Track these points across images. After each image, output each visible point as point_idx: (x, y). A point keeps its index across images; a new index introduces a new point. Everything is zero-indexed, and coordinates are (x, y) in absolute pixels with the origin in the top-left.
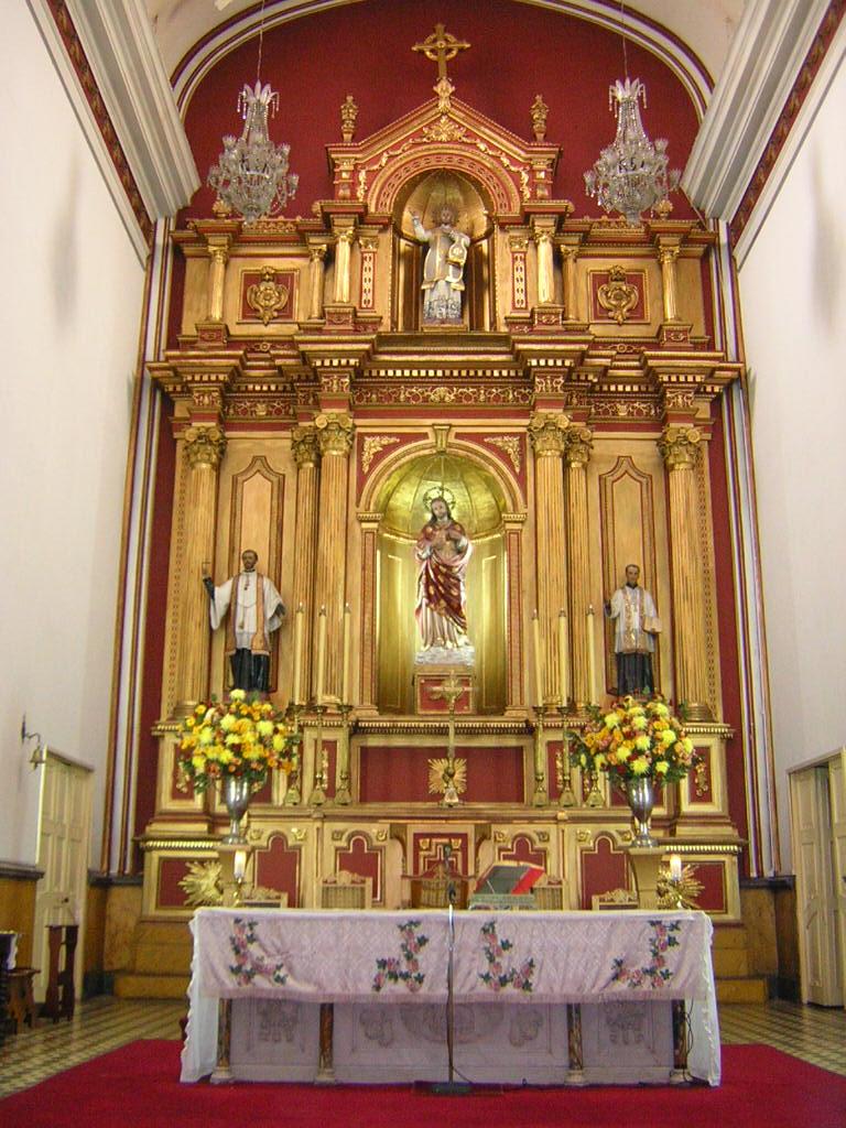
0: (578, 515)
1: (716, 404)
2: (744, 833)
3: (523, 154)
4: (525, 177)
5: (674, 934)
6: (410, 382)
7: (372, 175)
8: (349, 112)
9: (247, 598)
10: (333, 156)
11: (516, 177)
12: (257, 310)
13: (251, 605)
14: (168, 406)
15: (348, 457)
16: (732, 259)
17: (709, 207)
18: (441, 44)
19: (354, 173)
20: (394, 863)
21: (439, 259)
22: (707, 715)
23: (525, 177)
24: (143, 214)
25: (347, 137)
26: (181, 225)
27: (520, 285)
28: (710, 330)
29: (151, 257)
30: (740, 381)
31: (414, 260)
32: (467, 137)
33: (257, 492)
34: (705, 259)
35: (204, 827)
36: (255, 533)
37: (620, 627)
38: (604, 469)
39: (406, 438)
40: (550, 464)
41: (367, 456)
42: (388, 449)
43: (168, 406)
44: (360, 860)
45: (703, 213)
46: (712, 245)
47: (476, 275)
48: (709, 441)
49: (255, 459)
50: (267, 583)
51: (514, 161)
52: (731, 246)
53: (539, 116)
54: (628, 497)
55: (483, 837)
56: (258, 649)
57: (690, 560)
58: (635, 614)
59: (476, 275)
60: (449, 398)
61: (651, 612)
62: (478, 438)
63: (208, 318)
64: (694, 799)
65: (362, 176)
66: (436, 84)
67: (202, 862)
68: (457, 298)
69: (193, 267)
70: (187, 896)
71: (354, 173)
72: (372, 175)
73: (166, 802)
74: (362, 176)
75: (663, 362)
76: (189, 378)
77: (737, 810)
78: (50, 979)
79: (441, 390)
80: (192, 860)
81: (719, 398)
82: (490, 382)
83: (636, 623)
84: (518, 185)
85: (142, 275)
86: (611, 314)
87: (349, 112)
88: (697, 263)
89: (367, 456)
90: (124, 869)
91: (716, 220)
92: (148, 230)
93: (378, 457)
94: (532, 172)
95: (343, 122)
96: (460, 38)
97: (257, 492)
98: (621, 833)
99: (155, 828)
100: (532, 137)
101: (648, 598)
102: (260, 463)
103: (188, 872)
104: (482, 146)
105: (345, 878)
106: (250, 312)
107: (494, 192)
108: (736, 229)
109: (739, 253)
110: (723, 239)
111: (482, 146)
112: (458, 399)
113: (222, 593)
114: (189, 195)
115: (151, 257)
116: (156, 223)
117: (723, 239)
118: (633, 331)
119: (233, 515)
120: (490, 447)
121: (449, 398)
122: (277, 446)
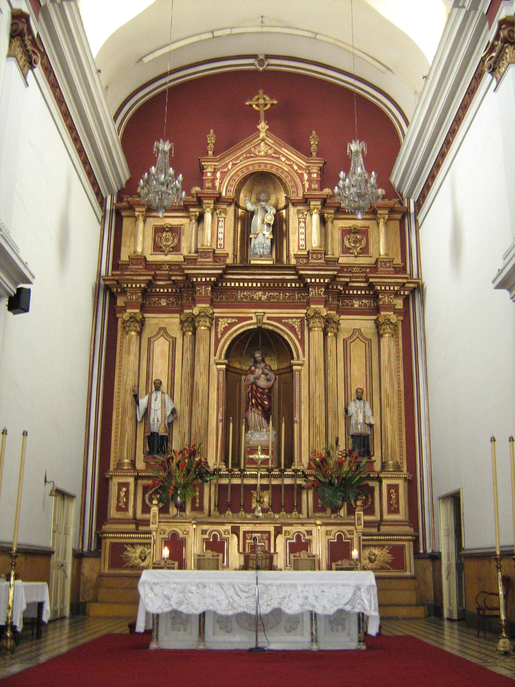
2: (416, 530)
3: (305, 164)
4: (306, 177)
6: (244, 289)
7: (224, 174)
8: (211, 139)
9: (156, 405)
10: (203, 164)
11: (301, 176)
12: (161, 247)
13: (159, 407)
14: (113, 298)
15: (210, 329)
16: (416, 221)
17: (405, 192)
18: (261, 101)
19: (214, 173)
21: (259, 221)
23: (306, 177)
24: (100, 195)
25: (211, 153)
26: (120, 199)
27: (302, 237)
28: (404, 260)
29: (104, 217)
30: (418, 289)
31: (246, 220)
32: (275, 153)
33: (161, 346)
34: (402, 221)
36: (160, 370)
37: (353, 421)
38: (346, 335)
39: (241, 320)
40: (317, 335)
41: (221, 328)
43: (113, 298)
45: (401, 195)
46: (406, 213)
47: (279, 230)
48: (402, 321)
49: (160, 329)
50: (167, 397)
51: (300, 168)
52: (416, 213)
53: (314, 142)
54: (358, 351)
55: (278, 531)
57: (391, 384)
58: (360, 412)
59: (279, 230)
61: (369, 413)
62: (279, 320)
63: (135, 252)
64: (390, 512)
65: (218, 175)
66: (259, 124)
67: (133, 545)
68: (269, 242)
69: (127, 223)
70: (124, 563)
71: (214, 173)
72: (224, 174)
73: (113, 513)
74: (218, 175)
75: (377, 280)
76: (125, 286)
79: (260, 293)
80: (127, 544)
81: (408, 297)
82: (286, 290)
83: (361, 419)
84: (302, 181)
85: (99, 227)
86: (351, 251)
87: (211, 139)
88: (398, 223)
89: (221, 328)
90: (91, 548)
91: (409, 199)
92: (102, 202)
93: (226, 329)
94: (309, 174)
95: (208, 144)
96: (271, 98)
97: (161, 346)
98: (349, 531)
99: (107, 527)
100: (309, 155)
101: (368, 405)
102: (163, 331)
103: (126, 550)
104: (283, 159)
105: (209, 554)
106: (157, 248)
108: (419, 205)
109: (420, 219)
110: (412, 210)
111: (283, 159)
112: (269, 298)
113: (143, 402)
114: (124, 182)
115: (104, 217)
116: (106, 198)
117: (412, 210)
118: (363, 260)
119: (148, 360)
120: (285, 324)
121: (264, 298)
122: (172, 322)
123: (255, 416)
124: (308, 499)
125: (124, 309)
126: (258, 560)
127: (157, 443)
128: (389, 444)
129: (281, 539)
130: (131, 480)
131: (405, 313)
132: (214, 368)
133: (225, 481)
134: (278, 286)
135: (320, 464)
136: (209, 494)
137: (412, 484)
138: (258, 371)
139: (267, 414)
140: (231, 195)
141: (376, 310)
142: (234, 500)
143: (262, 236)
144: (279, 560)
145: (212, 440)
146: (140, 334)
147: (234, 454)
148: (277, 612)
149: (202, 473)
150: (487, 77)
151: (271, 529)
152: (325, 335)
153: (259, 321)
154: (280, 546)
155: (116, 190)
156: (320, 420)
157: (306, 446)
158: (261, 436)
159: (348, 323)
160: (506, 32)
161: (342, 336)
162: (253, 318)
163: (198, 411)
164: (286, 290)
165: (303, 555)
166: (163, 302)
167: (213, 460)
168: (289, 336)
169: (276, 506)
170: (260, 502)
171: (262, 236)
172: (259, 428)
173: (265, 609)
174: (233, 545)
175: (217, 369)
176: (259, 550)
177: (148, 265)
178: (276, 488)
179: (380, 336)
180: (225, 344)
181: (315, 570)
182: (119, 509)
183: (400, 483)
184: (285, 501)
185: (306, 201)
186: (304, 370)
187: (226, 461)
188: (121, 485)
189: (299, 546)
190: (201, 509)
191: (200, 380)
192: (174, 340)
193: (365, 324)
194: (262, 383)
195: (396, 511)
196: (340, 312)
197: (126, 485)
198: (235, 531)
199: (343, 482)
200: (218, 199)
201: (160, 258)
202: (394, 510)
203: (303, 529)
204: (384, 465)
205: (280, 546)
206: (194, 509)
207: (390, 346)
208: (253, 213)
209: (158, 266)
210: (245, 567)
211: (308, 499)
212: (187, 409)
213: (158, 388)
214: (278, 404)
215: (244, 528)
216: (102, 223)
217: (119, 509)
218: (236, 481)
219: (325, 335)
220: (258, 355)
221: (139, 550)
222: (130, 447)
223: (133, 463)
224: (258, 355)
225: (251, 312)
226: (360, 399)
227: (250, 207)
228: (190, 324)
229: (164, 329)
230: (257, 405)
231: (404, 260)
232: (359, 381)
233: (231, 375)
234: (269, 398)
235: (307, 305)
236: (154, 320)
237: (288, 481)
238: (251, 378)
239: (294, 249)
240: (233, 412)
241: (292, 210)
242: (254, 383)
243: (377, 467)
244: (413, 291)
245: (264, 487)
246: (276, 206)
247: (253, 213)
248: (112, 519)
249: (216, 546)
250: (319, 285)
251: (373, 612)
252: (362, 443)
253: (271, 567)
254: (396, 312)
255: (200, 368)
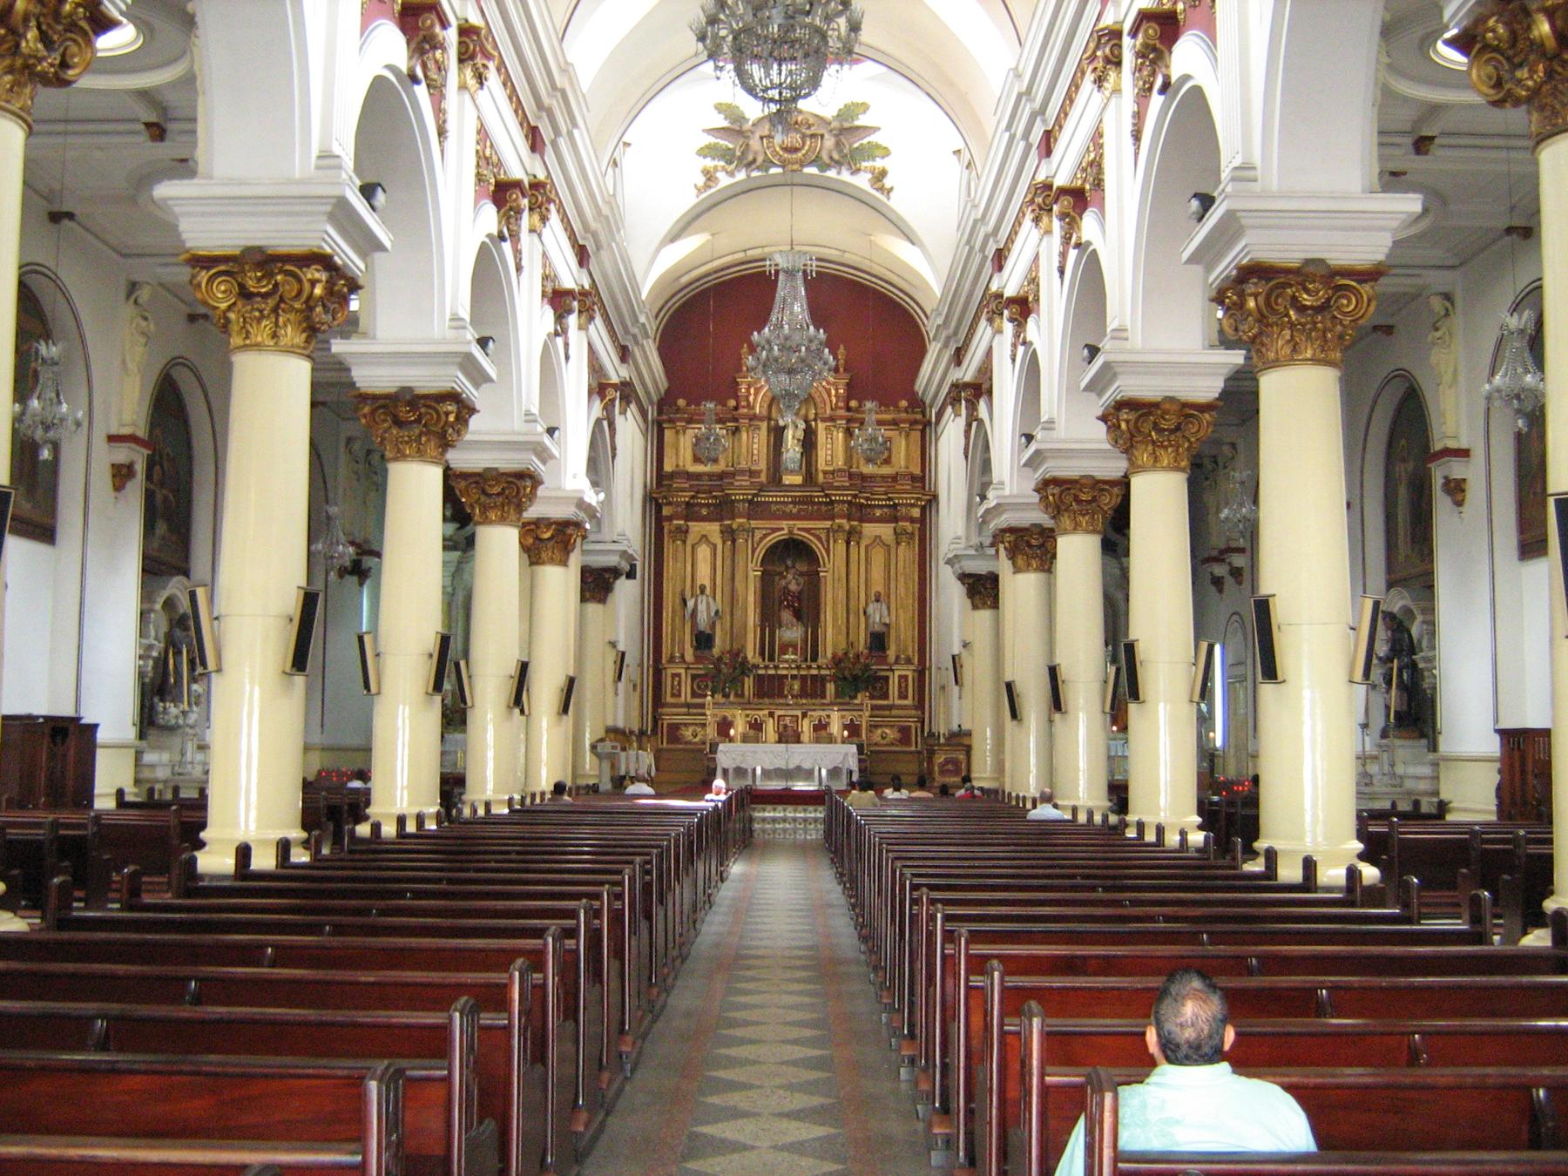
0: (853, 567)
1: (923, 509)
5: (1229, 582)
9: (702, 607)
14: (659, 508)
19: (748, 390)
20: (770, 727)
22: (909, 661)
26: (660, 412)
28: (923, 470)
31: (778, 433)
33: (704, 552)
34: (923, 432)
35: (685, 710)
36: (703, 574)
39: (774, 530)
40: (840, 547)
41: (757, 539)
42: (765, 536)
43: (659, 508)
44: (757, 726)
46: (929, 422)
47: (809, 443)
54: (878, 556)
55: (804, 715)
56: (708, 631)
57: (905, 589)
58: (877, 614)
59: (809, 443)
60: (795, 511)
61: (885, 612)
69: (668, 434)
71: (748, 390)
72: (757, 391)
77: (920, 704)
78: (1508, 957)
82: (814, 503)
89: (757, 539)
97: (704, 552)
105: (752, 732)
106: (697, 460)
107: (820, 405)
109: (940, 430)
113: (690, 604)
118: (886, 470)
121: (795, 511)
122: (713, 529)
123: (787, 616)
124: (830, 688)
125: (670, 519)
126: (788, 736)
127: (703, 641)
128: (902, 638)
129: (806, 721)
130: (682, 671)
131: (922, 520)
132: (752, 574)
133: (761, 672)
134: (808, 501)
135: (837, 661)
136: (749, 683)
137: (921, 673)
138: (790, 577)
139: (798, 615)
140: (765, 413)
141: (895, 520)
142: (770, 688)
143: (792, 449)
144: (805, 737)
145: (750, 636)
146: (684, 542)
147: (769, 650)
148: (799, 768)
149: (744, 668)
150: (949, 409)
151: (799, 713)
152: (848, 543)
153: (790, 532)
154: (806, 727)
155: (655, 399)
156: (841, 621)
157: (831, 639)
158: (792, 632)
159: (870, 530)
160: (1107, 50)
161: (863, 544)
162: (785, 529)
163: (738, 613)
164: (814, 503)
165: (823, 733)
166: (704, 512)
167: (751, 654)
168: (817, 546)
169: (803, 693)
170: (791, 689)
171: (792, 449)
172: (790, 626)
173: (791, 766)
174: (770, 727)
175: (755, 573)
176: (790, 731)
177: (690, 476)
178: (804, 678)
179: (898, 543)
180: (760, 552)
181: (1551, 857)
182: (673, 695)
183: (910, 674)
184: (812, 688)
185: (832, 419)
186: (829, 576)
187: (762, 654)
188: (674, 675)
189: (820, 727)
190: (742, 695)
191: (739, 586)
192: (715, 546)
193: (885, 531)
194: (793, 587)
195: (906, 697)
196: (861, 520)
197: (679, 675)
198: (771, 715)
199: (859, 676)
200: (753, 418)
201: (700, 468)
202: (903, 696)
203: (824, 714)
204: (898, 657)
205: (806, 727)
206: (736, 695)
207: (906, 555)
208: (784, 428)
209: (698, 476)
210: (780, 741)
211: (830, 688)
212: (728, 610)
213: (703, 592)
214: (807, 608)
215: (778, 713)
216: (645, 436)
217: (673, 695)
218: (772, 672)
219: (848, 543)
220: (789, 563)
221: (691, 729)
222: (680, 643)
223: (682, 656)
224: (789, 563)
225: (784, 524)
226: (877, 600)
227: (781, 423)
228: (730, 535)
229: (704, 536)
230: (788, 607)
231: (923, 470)
232: (878, 587)
233: (767, 580)
234: (799, 600)
235: (832, 518)
236: (696, 528)
237: (814, 672)
238: (783, 583)
239: (821, 465)
240: (768, 618)
241: (821, 426)
242: (786, 588)
243: (892, 659)
244: (930, 501)
245: (794, 677)
246: (806, 421)
247: (784, 428)
248: (1267, 867)
249: (757, 726)
250: (843, 502)
251: (855, 766)
252: (878, 641)
253: (798, 741)
254: (912, 520)
255: (739, 576)
